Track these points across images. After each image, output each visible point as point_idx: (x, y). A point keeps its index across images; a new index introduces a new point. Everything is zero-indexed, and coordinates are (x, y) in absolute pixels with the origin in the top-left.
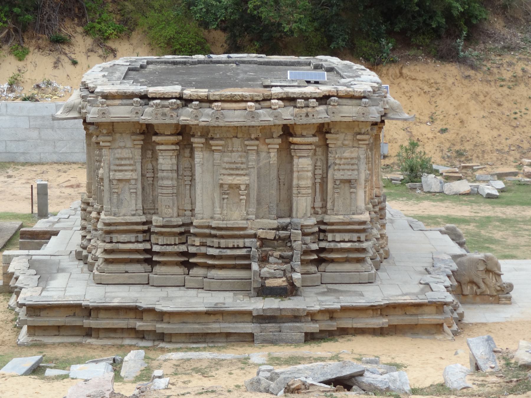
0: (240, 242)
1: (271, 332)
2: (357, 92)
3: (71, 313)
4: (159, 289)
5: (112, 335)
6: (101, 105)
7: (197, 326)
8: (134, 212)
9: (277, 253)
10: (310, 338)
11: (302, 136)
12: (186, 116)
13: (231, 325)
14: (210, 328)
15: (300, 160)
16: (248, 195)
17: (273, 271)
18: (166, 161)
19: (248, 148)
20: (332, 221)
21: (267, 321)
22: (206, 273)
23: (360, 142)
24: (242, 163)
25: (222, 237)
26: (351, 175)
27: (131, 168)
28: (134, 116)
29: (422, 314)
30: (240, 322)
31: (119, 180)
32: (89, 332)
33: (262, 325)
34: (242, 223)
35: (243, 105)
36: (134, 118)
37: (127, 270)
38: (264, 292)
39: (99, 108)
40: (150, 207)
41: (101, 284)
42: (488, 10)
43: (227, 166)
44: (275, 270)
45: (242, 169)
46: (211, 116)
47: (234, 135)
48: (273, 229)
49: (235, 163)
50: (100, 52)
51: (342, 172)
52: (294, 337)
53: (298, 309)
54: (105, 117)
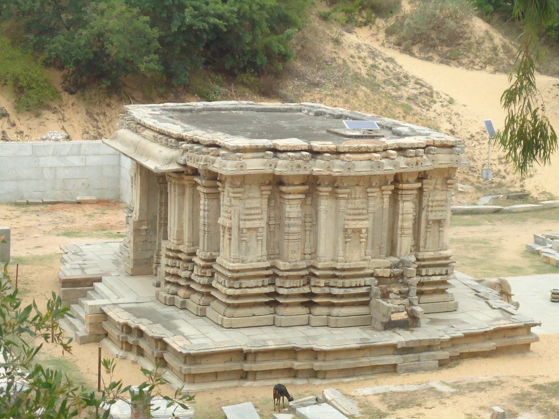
0: (361, 281)
1: (411, 362)
2: (449, 141)
3: (228, 359)
4: (289, 329)
5: (268, 376)
6: (238, 159)
7: (351, 362)
8: (260, 258)
9: (396, 290)
10: (442, 364)
11: (408, 182)
12: (318, 167)
13: (377, 358)
14: (362, 363)
15: (405, 204)
16: (367, 238)
17: (397, 306)
19: (369, 195)
20: (425, 257)
21: (406, 352)
22: (329, 311)
23: (449, 186)
24: (363, 209)
25: (344, 277)
26: (441, 216)
27: (259, 217)
28: (268, 168)
29: (517, 336)
30: (385, 355)
31: (249, 229)
32: (244, 375)
33: (405, 356)
34: (362, 264)
35: (367, 156)
36: (268, 170)
37: (254, 313)
38: (390, 325)
39: (237, 161)
40: (275, 252)
41: (231, 328)
42: (63, 45)
43: (352, 212)
44: (399, 305)
45: (363, 215)
46: (343, 167)
47: (357, 183)
48: (387, 268)
49: (358, 209)
51: (434, 214)
52: (430, 365)
53: (434, 340)
54: (243, 170)
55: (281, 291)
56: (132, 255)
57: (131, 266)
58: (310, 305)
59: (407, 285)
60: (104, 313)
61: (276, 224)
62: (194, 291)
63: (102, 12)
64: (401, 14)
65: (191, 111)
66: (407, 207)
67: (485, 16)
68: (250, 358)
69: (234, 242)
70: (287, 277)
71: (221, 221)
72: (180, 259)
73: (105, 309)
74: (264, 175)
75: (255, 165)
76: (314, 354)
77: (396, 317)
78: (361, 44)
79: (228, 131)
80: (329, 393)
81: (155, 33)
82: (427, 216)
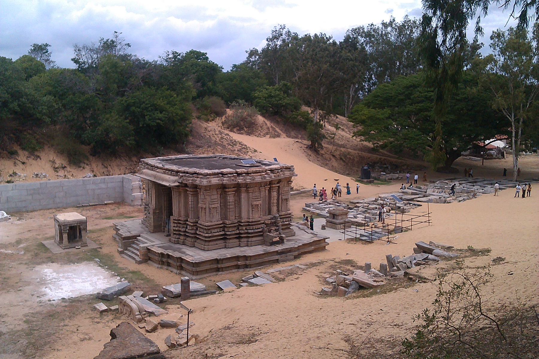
0: (260, 226)
12: (240, 180)
18: (231, 198)
25: (252, 225)
32: (218, 270)
34: (259, 219)
35: (259, 174)
40: (224, 217)
50: (33, 157)
55: (228, 233)
56: (152, 224)
57: (153, 229)
58: (239, 238)
59: (277, 226)
60: (149, 249)
61: (224, 205)
62: (188, 236)
63: (107, 119)
64: (227, 115)
65: (170, 160)
66: (274, 194)
67: (263, 115)
68: (220, 262)
69: (207, 214)
70: (230, 227)
71: (200, 205)
72: (180, 223)
73: (149, 248)
74: (218, 185)
75: (215, 181)
76: (246, 258)
77: (275, 240)
78: (213, 127)
79: (161, 169)
80: (257, 273)
81: (131, 127)
82: (282, 198)
